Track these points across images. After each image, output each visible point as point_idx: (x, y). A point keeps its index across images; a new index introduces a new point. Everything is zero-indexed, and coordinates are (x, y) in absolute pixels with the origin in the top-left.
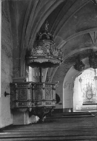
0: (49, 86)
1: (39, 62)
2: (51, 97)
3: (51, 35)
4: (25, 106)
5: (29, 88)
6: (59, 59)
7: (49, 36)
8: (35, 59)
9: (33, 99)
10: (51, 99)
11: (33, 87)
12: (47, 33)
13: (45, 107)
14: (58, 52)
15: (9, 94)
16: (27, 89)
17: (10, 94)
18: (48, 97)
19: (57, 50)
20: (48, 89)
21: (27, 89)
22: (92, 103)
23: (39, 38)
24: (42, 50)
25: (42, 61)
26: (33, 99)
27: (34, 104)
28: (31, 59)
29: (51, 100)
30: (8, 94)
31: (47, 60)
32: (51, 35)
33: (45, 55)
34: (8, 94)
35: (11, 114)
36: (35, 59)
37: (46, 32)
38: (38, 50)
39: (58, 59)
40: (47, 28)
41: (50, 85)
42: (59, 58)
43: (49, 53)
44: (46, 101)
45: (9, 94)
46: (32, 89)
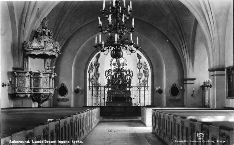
0: (46, 75)
1: (35, 54)
2: (48, 85)
3: (50, 31)
4: (24, 92)
5: (27, 77)
6: (54, 51)
7: (47, 32)
8: (31, 51)
9: (31, 86)
10: (48, 87)
11: (32, 75)
12: (46, 30)
13: (43, 93)
14: (53, 45)
15: (7, 85)
16: (25, 77)
17: (9, 85)
18: (45, 85)
19: (51, 43)
20: (45, 78)
21: (25, 77)
22: (124, 114)
23: (38, 34)
24: (37, 43)
25: (38, 53)
26: (31, 86)
27: (32, 91)
28: (28, 51)
29: (48, 88)
30: (5, 85)
31: (42, 53)
32: (50, 31)
33: (40, 48)
34: (5, 85)
35: (10, 100)
36: (31, 51)
37: (44, 29)
38: (33, 44)
39: (53, 51)
40: (46, 24)
41: (47, 74)
42: (54, 51)
43: (43, 46)
44: (43, 89)
45: (7, 85)
46: (31, 77)
